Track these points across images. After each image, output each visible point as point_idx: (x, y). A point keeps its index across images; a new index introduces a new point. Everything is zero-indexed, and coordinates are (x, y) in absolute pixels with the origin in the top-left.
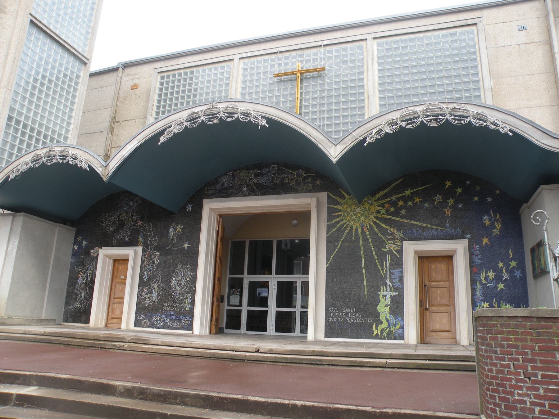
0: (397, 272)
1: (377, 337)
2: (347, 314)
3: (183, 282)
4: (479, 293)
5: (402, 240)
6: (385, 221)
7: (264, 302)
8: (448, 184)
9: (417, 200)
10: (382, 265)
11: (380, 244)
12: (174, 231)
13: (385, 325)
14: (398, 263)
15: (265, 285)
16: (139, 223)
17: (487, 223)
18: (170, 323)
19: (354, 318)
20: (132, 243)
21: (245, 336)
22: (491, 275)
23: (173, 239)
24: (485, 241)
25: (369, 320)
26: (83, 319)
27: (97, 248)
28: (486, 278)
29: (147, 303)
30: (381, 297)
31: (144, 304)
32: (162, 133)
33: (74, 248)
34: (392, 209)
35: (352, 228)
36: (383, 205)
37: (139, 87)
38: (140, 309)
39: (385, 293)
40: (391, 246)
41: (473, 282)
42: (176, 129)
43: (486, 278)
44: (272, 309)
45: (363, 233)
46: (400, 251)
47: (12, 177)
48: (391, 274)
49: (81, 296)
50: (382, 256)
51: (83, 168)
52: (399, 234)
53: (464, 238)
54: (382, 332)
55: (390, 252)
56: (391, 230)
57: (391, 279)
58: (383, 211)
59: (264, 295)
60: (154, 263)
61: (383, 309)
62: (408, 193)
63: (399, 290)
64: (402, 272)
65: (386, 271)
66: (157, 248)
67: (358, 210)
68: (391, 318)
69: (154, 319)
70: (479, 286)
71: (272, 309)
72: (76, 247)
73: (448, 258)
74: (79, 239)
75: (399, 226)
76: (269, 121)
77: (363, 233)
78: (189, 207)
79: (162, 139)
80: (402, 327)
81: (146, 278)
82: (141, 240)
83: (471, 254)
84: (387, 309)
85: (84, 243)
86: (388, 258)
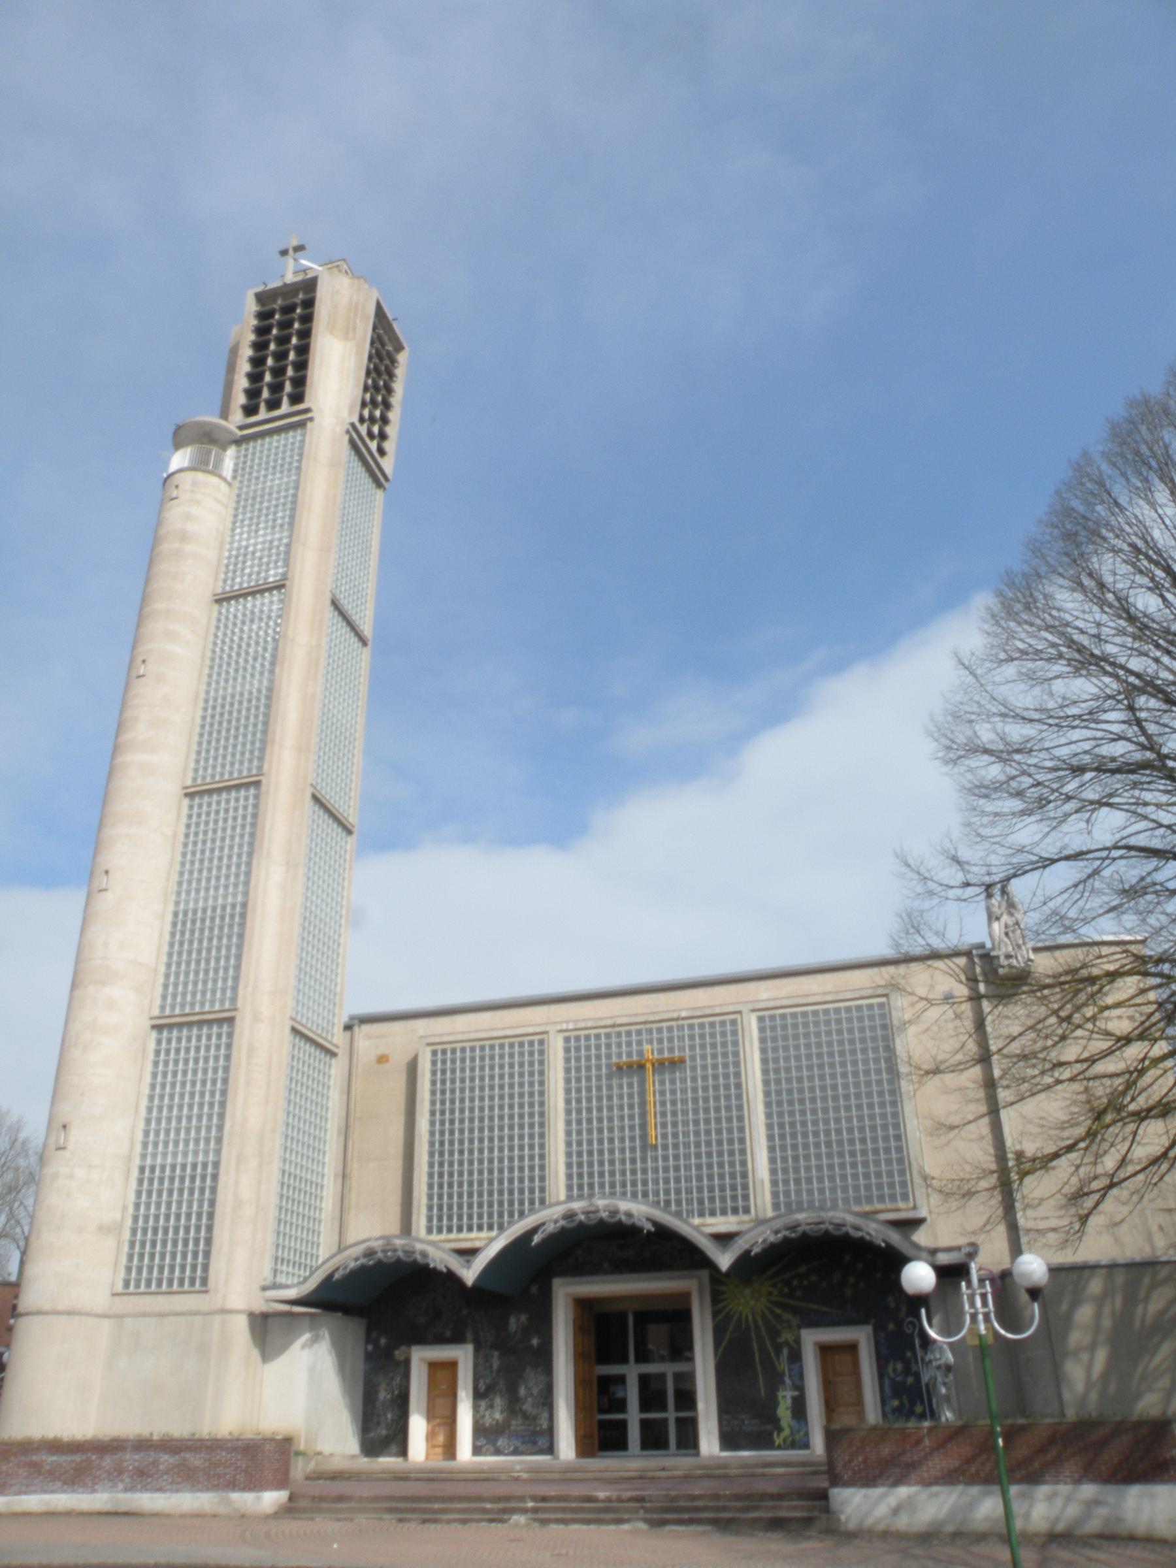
0: (796, 1366)
1: (779, 1448)
2: (743, 1421)
3: (535, 1391)
4: (887, 1390)
5: (800, 1327)
6: (777, 1304)
7: (621, 1406)
8: (847, 1258)
9: (814, 1278)
10: (778, 1359)
11: (774, 1334)
12: (515, 1323)
13: (786, 1432)
14: (796, 1356)
15: (621, 1380)
16: (465, 1312)
17: (892, 1305)
18: (522, 1448)
19: (750, 1425)
20: (457, 1339)
21: (674, 1455)
22: (899, 1366)
23: (516, 1333)
24: (891, 1326)
25: (769, 1427)
26: (394, 1448)
27: (403, 1348)
28: (895, 1370)
29: (488, 1421)
30: (780, 1398)
31: (483, 1424)
32: (534, 1230)
33: (366, 1349)
34: (786, 1290)
35: (741, 1314)
36: (775, 1285)
37: (390, 1058)
38: (479, 1430)
39: (785, 1393)
40: (787, 1336)
41: (881, 1374)
42: (551, 1228)
43: (895, 1370)
44: (634, 1417)
45: (755, 1321)
46: (798, 1341)
47: (337, 1276)
48: (790, 1370)
49: (386, 1419)
50: (778, 1348)
51: (432, 1266)
52: (795, 1321)
53: (866, 1322)
54: (785, 1440)
55: (787, 1343)
56: (787, 1316)
57: (790, 1377)
58: (775, 1292)
59: (620, 1394)
60: (491, 1366)
61: (784, 1412)
62: (803, 1269)
63: (800, 1388)
64: (801, 1367)
65: (783, 1366)
66: (495, 1346)
67: (747, 1292)
68: (794, 1423)
69: (499, 1443)
70: (887, 1381)
71: (634, 1417)
72: (370, 1347)
73: (852, 1348)
74: (374, 1335)
75: (795, 1311)
76: (655, 1224)
77: (755, 1321)
78: (534, 1290)
79: (536, 1239)
80: (807, 1434)
81: (482, 1387)
82: (469, 1335)
83: (877, 1343)
84: (789, 1413)
85: (383, 1341)
86: (785, 1351)
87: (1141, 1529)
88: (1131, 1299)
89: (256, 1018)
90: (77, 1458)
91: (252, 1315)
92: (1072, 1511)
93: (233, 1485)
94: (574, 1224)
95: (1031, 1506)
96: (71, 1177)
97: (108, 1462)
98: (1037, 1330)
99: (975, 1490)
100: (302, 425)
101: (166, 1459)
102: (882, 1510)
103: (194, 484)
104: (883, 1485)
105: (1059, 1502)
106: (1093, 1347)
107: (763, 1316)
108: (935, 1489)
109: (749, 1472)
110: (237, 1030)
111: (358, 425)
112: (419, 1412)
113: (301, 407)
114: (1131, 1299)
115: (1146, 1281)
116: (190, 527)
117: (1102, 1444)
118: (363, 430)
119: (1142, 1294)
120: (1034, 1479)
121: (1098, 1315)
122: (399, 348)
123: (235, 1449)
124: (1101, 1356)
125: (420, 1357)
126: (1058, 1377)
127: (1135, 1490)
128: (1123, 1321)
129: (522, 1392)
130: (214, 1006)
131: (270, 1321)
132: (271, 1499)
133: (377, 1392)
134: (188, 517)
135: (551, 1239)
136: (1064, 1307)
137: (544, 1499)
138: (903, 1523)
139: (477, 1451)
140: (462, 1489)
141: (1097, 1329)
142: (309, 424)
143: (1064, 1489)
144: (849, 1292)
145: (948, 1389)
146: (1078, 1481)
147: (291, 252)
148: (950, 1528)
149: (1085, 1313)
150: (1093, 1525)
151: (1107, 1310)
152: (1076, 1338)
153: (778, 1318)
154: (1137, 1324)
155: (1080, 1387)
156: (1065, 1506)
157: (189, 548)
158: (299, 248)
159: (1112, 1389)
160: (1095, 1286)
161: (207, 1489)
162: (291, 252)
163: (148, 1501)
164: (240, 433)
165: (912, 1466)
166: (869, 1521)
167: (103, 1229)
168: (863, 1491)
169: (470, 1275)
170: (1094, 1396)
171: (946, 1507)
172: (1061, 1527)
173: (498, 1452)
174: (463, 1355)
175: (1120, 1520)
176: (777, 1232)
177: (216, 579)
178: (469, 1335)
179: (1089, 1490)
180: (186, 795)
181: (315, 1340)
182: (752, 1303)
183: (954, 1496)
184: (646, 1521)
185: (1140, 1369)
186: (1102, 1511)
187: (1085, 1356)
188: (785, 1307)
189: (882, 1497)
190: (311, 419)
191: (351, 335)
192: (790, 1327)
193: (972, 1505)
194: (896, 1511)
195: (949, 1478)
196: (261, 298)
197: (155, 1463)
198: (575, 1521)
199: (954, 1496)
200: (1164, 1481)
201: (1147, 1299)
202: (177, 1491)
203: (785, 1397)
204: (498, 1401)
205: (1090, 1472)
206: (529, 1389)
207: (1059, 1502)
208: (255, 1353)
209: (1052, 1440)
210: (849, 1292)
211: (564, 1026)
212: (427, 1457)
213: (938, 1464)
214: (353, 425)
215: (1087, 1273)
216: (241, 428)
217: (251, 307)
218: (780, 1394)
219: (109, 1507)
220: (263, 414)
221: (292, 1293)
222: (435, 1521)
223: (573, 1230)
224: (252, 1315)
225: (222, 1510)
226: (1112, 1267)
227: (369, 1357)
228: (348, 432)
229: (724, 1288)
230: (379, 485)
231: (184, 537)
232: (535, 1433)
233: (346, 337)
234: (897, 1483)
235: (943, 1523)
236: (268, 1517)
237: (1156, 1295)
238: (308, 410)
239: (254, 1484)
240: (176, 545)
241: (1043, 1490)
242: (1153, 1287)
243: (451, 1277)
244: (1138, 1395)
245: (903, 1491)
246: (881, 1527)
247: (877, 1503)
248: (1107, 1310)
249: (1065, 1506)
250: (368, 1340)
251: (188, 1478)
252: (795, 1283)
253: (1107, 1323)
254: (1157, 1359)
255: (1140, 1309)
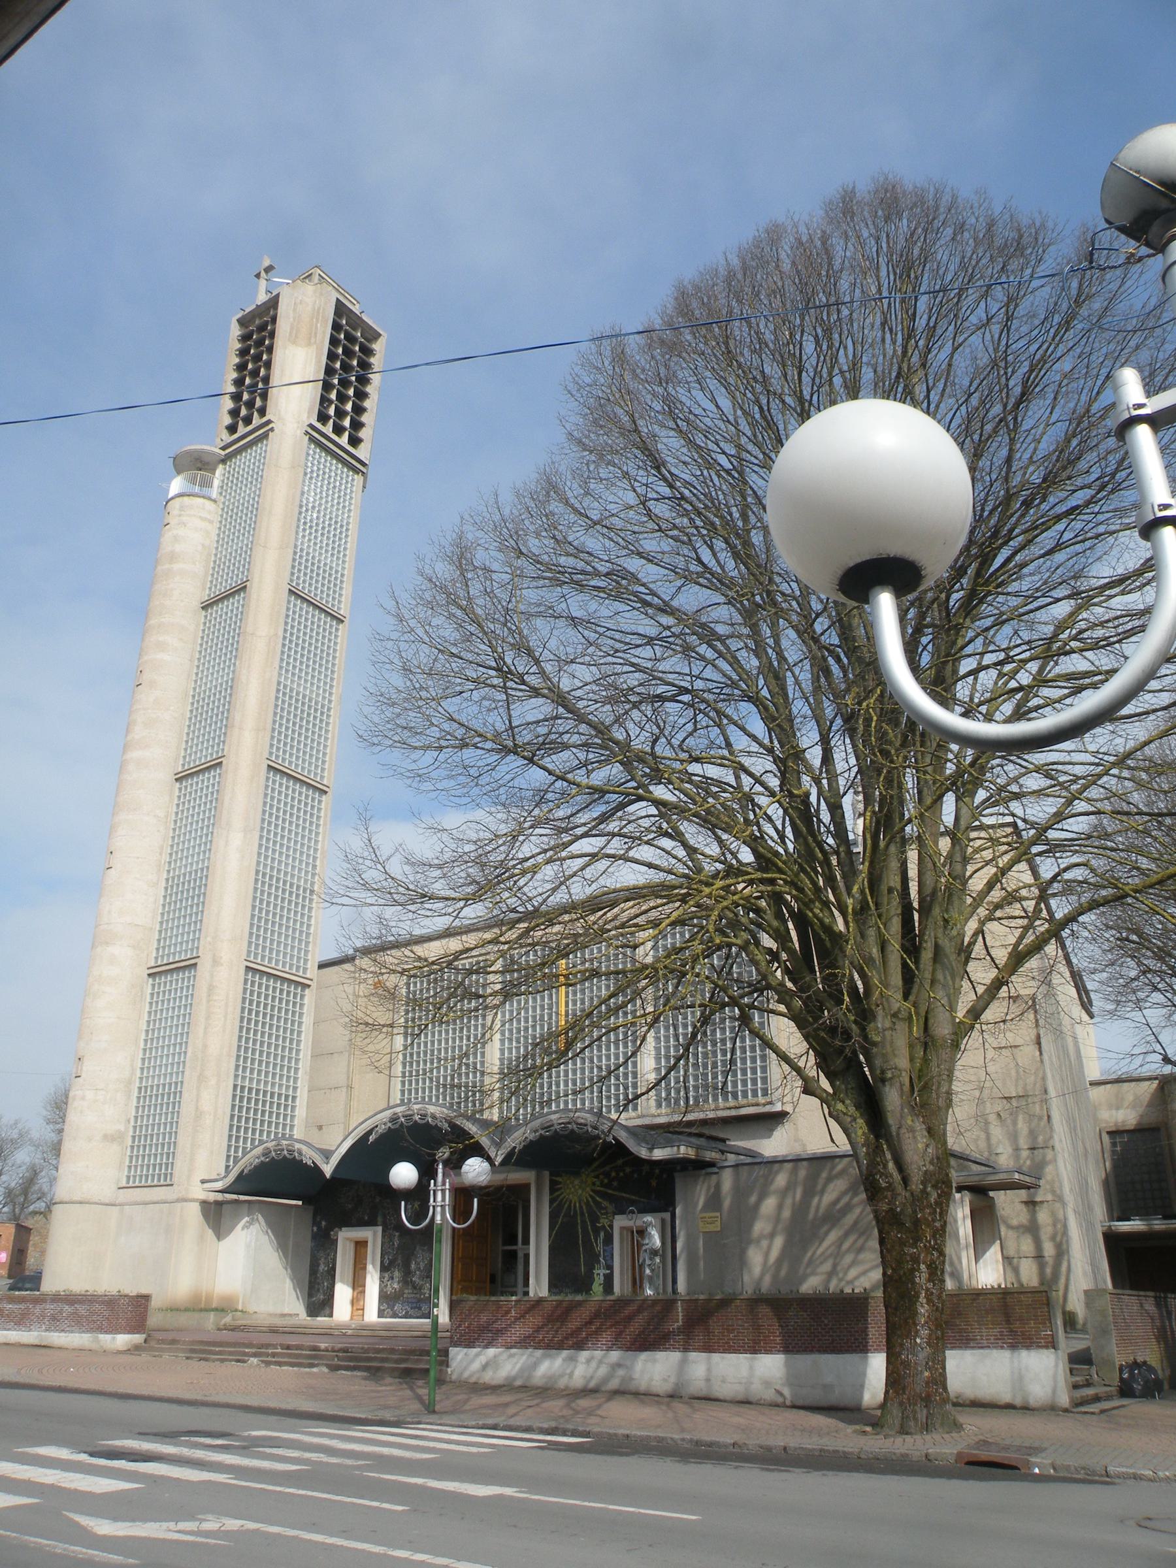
3: (422, 1266)
5: (615, 1214)
9: (628, 1170)
11: (595, 1219)
18: (411, 1312)
20: (371, 1223)
29: (389, 1290)
32: (369, 1133)
34: (606, 1181)
36: (597, 1177)
38: (384, 1297)
40: (604, 1221)
42: (382, 1129)
45: (581, 1207)
46: (611, 1227)
50: (596, 1231)
56: (605, 1203)
58: (598, 1183)
65: (600, 1248)
67: (577, 1182)
72: (315, 1229)
77: (581, 1207)
79: (372, 1138)
81: (386, 1262)
82: (380, 1219)
84: (601, 1289)
85: (324, 1223)
86: (602, 1234)
87: (643, 1387)
88: (810, 1191)
89: (216, 962)
90: (22, 1306)
91: (204, 1204)
92: (603, 1371)
93: (101, 1329)
94: (397, 1126)
95: (575, 1367)
96: (83, 1098)
97: (38, 1310)
98: (473, 1222)
99: (539, 1353)
100: (265, 436)
101: (67, 1308)
102: (476, 1366)
103: (182, 508)
104: (479, 1346)
105: (594, 1364)
106: (772, 1236)
107: (587, 1203)
108: (514, 1351)
109: (388, 1328)
110: (199, 974)
111: (318, 425)
112: (342, 1281)
113: (265, 419)
114: (810, 1191)
115: (824, 1175)
116: (178, 548)
117: (630, 1318)
118: (328, 429)
119: (819, 1187)
120: (579, 1346)
121: (780, 1207)
122: (376, 336)
123: (103, 1302)
124: (779, 1242)
125: (345, 1237)
126: (743, 1262)
127: (644, 1356)
128: (801, 1210)
129: (413, 1266)
130: (181, 955)
131: (224, 1206)
132: (122, 1340)
133: (318, 1265)
134: (176, 539)
135: (383, 1138)
136: (753, 1199)
137: (288, 1347)
138: (488, 1377)
139: (381, 1314)
140: (257, 1338)
141: (778, 1219)
142: (271, 434)
143: (598, 1354)
144: (654, 1183)
145: (652, 1271)
146: (609, 1349)
147: (263, 274)
148: (518, 1383)
149: (769, 1205)
150: (614, 1384)
151: (789, 1202)
152: (760, 1227)
153: (597, 1204)
154: (811, 1216)
155: (757, 1270)
156: (598, 1367)
157: (176, 566)
158: (268, 269)
159: (783, 1273)
160: (781, 1180)
161: (87, 1332)
162: (263, 274)
163: (58, 1338)
164: (223, 453)
165: (500, 1332)
166: (466, 1375)
167: (109, 1138)
168: (465, 1350)
169: (328, 1170)
170: (767, 1280)
171: (518, 1366)
172: (592, 1385)
173: (395, 1316)
174: (373, 1236)
175: (631, 1379)
176: (536, 1131)
177: (204, 589)
179: (615, 1355)
180: (177, 780)
181: (251, 1223)
182: (580, 1192)
183: (524, 1357)
184: (328, 1366)
185: (809, 1254)
186: (621, 1372)
187: (765, 1243)
188: (603, 1195)
189: (477, 1355)
190: (272, 430)
191: (313, 340)
192: (606, 1213)
193: (535, 1365)
194: (485, 1367)
195: (524, 1343)
196: (242, 322)
197: (61, 1312)
198: (286, 1364)
199: (524, 1357)
200: (666, 1349)
201: (822, 1192)
202: (72, 1332)
203: (600, 1273)
204: (397, 1274)
205: (616, 1343)
206: (417, 1264)
207: (594, 1364)
208: (210, 1233)
209: (596, 1315)
210: (654, 1183)
212: (352, 1319)
213: (519, 1331)
214: (311, 426)
215: (776, 1166)
216: (223, 448)
217: (236, 331)
218: (596, 1272)
219: (36, 1342)
220: (242, 429)
221: (219, 1185)
222: (206, 1360)
223: (396, 1130)
224: (204, 1204)
225: (94, 1346)
226: (797, 1160)
227: (314, 1237)
228: (307, 433)
229: (560, 1179)
230: (356, 471)
231: (173, 557)
232: (420, 1300)
233: (309, 344)
234: (486, 1347)
235: (515, 1378)
236: (119, 1352)
237: (831, 1186)
238: (269, 422)
239: (113, 1329)
240: (167, 566)
241: (584, 1355)
242: (830, 1179)
243: (317, 1170)
244: (804, 1278)
245: (491, 1352)
246: (473, 1380)
247: (472, 1361)
248: (789, 1202)
249: (598, 1367)
250: (314, 1223)
251: (80, 1323)
252: (613, 1174)
253: (787, 1214)
254: (826, 1244)
255: (816, 1200)
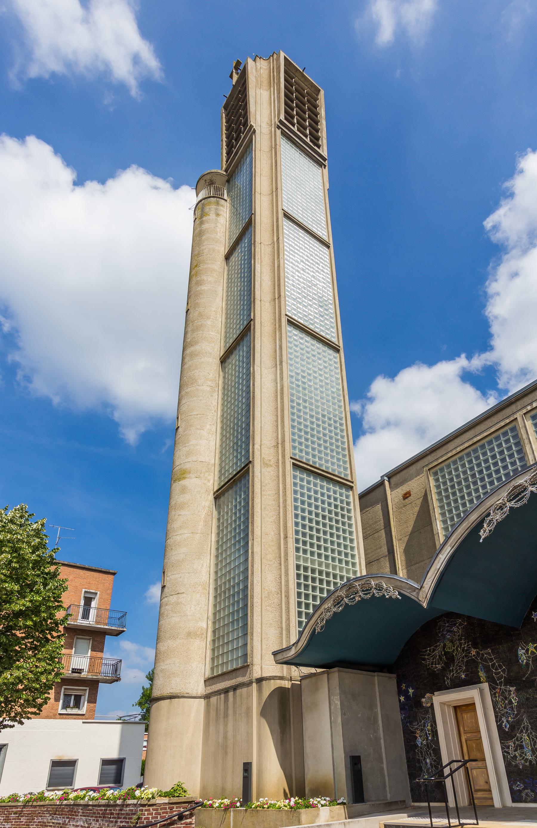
47: (318, 630)
60: (511, 702)
66: (509, 682)
72: (402, 698)
82: (482, 674)
85: (411, 691)
178: (482, 674)
211: (529, 408)
250: (400, 692)
